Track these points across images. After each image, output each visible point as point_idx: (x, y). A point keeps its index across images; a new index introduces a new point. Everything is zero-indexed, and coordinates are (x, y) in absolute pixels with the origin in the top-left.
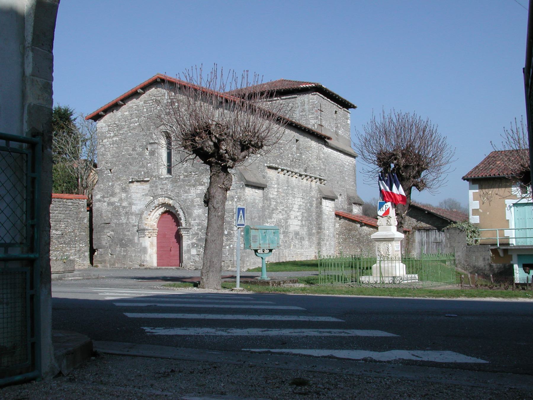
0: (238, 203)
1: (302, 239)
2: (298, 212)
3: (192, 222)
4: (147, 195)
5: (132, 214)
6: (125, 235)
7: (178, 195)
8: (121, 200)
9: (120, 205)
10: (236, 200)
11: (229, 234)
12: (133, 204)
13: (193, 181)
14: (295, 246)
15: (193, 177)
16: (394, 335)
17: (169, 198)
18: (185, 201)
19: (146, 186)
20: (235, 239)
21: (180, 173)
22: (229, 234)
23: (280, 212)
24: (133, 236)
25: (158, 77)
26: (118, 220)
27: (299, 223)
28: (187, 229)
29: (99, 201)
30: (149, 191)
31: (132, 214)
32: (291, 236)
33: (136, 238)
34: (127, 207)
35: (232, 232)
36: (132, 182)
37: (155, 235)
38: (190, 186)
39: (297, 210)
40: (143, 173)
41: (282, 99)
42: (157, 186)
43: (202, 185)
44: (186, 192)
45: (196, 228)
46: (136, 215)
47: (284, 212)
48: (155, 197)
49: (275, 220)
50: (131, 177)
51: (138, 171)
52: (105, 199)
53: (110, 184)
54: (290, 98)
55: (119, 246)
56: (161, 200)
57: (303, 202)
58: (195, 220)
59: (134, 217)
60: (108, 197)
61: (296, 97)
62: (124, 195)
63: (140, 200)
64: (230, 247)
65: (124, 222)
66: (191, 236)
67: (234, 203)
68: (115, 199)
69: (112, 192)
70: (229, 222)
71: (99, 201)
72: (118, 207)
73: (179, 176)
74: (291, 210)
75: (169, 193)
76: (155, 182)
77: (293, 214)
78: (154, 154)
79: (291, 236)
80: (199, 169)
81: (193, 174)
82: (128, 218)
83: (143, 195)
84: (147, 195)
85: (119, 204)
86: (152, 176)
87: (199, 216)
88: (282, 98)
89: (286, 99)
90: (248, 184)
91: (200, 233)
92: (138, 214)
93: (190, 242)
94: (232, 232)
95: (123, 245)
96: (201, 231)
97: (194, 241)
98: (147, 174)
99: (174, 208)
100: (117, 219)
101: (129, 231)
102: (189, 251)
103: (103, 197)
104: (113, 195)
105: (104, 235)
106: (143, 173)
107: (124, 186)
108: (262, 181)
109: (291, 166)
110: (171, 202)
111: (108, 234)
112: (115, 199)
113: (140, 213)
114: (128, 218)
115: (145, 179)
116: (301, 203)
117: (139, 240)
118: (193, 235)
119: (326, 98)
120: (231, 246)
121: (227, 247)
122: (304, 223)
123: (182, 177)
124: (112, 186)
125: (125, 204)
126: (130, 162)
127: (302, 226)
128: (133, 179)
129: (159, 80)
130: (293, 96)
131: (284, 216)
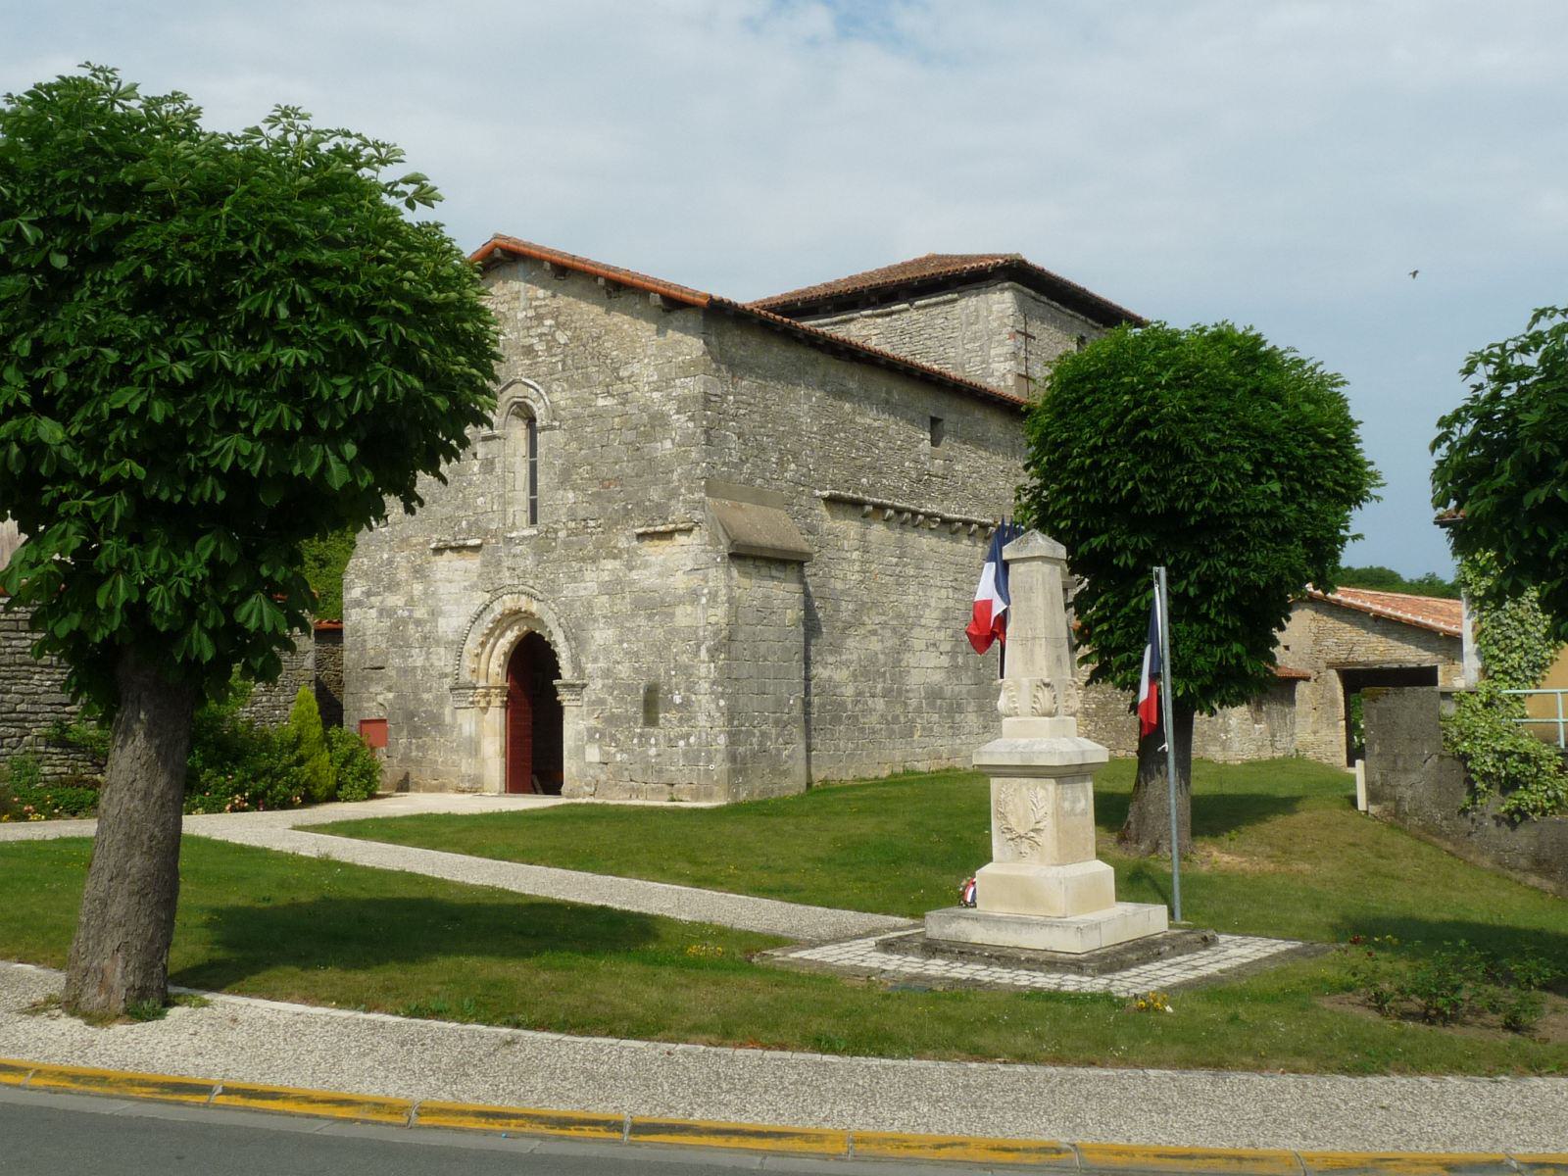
0: (711, 611)
1: (955, 708)
2: (939, 628)
3: (589, 667)
4: (473, 587)
5: (438, 642)
6: (420, 701)
7: (552, 589)
8: (411, 602)
9: (410, 617)
10: (704, 600)
11: (686, 704)
12: (441, 613)
13: (590, 547)
14: (931, 730)
15: (592, 534)
16: (1290, 945)
17: (530, 595)
18: (569, 605)
19: (473, 563)
20: (702, 721)
21: (556, 522)
22: (686, 704)
23: (874, 633)
24: (440, 700)
25: (496, 246)
26: (404, 657)
27: (945, 661)
28: (577, 688)
29: (358, 603)
30: (480, 575)
31: (438, 642)
32: (913, 703)
33: (447, 710)
34: (426, 622)
35: (693, 697)
36: (438, 551)
37: (497, 701)
38: (583, 559)
39: (937, 623)
40: (464, 523)
41: (918, 308)
42: (499, 563)
43: (615, 558)
44: (574, 579)
45: (599, 683)
46: (449, 644)
47: (888, 633)
48: (496, 592)
49: (855, 657)
50: (436, 536)
51: (450, 519)
52: (372, 599)
53: (385, 556)
54: (936, 304)
55: (405, 732)
56: (509, 602)
57: (957, 600)
58: (595, 660)
59: (442, 651)
60: (379, 594)
61: (955, 301)
62: (418, 588)
63: (457, 602)
64: (688, 744)
65: (419, 662)
66: (585, 708)
67: (699, 610)
68: (394, 600)
69: (391, 580)
70: (687, 667)
71: (358, 603)
72: (404, 622)
73: (556, 531)
74: (913, 625)
75: (531, 583)
76: (496, 549)
77: (918, 638)
78: (493, 469)
79: (913, 703)
80: (606, 509)
81: (592, 523)
82: (428, 653)
83: (465, 588)
84: (473, 587)
85: (406, 614)
86: (487, 532)
87: (606, 650)
88: (918, 303)
89: (926, 306)
90: (743, 551)
91: (610, 699)
92: (453, 642)
93: (582, 725)
94: (693, 697)
95: (415, 732)
96: (611, 694)
97: (593, 722)
98: (475, 527)
99: (540, 621)
100: (403, 657)
101: (429, 690)
102: (580, 751)
103: (368, 594)
104: (393, 586)
105: (369, 700)
106: (464, 523)
107: (419, 562)
108: (797, 541)
109: (912, 495)
110: (534, 607)
111: (380, 699)
112: (394, 600)
113: (456, 638)
114: (428, 653)
115: (470, 542)
116: (951, 603)
117: (453, 714)
118: (591, 703)
119: (1044, 299)
120: (692, 740)
121: (682, 743)
122: (960, 660)
123: (562, 534)
124: (390, 562)
125: (420, 613)
126: (433, 494)
127: (954, 670)
128: (440, 540)
129: (498, 253)
130: (946, 298)
131: (889, 644)
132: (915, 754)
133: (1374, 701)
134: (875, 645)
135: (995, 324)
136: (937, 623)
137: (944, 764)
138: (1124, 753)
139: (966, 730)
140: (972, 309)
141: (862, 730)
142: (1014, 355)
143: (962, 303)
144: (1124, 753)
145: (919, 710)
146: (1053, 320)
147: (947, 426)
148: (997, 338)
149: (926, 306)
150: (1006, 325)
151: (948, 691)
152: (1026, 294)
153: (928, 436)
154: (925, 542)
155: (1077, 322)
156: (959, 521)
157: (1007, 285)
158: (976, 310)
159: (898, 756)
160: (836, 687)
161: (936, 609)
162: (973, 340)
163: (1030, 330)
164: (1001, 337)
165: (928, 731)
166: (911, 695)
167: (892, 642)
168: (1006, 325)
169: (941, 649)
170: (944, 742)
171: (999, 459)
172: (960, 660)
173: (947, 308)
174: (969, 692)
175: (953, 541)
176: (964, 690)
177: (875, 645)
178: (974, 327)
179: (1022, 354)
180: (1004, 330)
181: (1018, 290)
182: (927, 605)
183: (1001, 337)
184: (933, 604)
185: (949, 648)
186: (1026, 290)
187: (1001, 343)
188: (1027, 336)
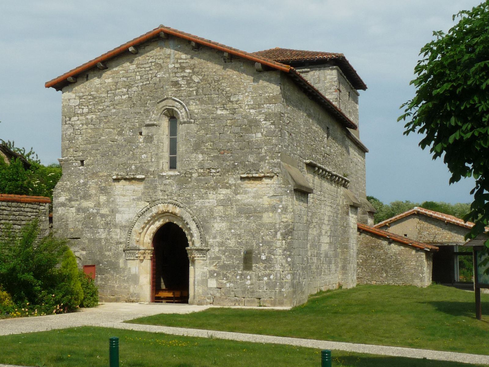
61: (308, 72)
135: (328, 85)
138: (375, 282)
140: (317, 76)
148: (329, 91)
150: (333, 85)
157: (335, 67)
158: (319, 77)
164: (331, 91)
168: (333, 85)
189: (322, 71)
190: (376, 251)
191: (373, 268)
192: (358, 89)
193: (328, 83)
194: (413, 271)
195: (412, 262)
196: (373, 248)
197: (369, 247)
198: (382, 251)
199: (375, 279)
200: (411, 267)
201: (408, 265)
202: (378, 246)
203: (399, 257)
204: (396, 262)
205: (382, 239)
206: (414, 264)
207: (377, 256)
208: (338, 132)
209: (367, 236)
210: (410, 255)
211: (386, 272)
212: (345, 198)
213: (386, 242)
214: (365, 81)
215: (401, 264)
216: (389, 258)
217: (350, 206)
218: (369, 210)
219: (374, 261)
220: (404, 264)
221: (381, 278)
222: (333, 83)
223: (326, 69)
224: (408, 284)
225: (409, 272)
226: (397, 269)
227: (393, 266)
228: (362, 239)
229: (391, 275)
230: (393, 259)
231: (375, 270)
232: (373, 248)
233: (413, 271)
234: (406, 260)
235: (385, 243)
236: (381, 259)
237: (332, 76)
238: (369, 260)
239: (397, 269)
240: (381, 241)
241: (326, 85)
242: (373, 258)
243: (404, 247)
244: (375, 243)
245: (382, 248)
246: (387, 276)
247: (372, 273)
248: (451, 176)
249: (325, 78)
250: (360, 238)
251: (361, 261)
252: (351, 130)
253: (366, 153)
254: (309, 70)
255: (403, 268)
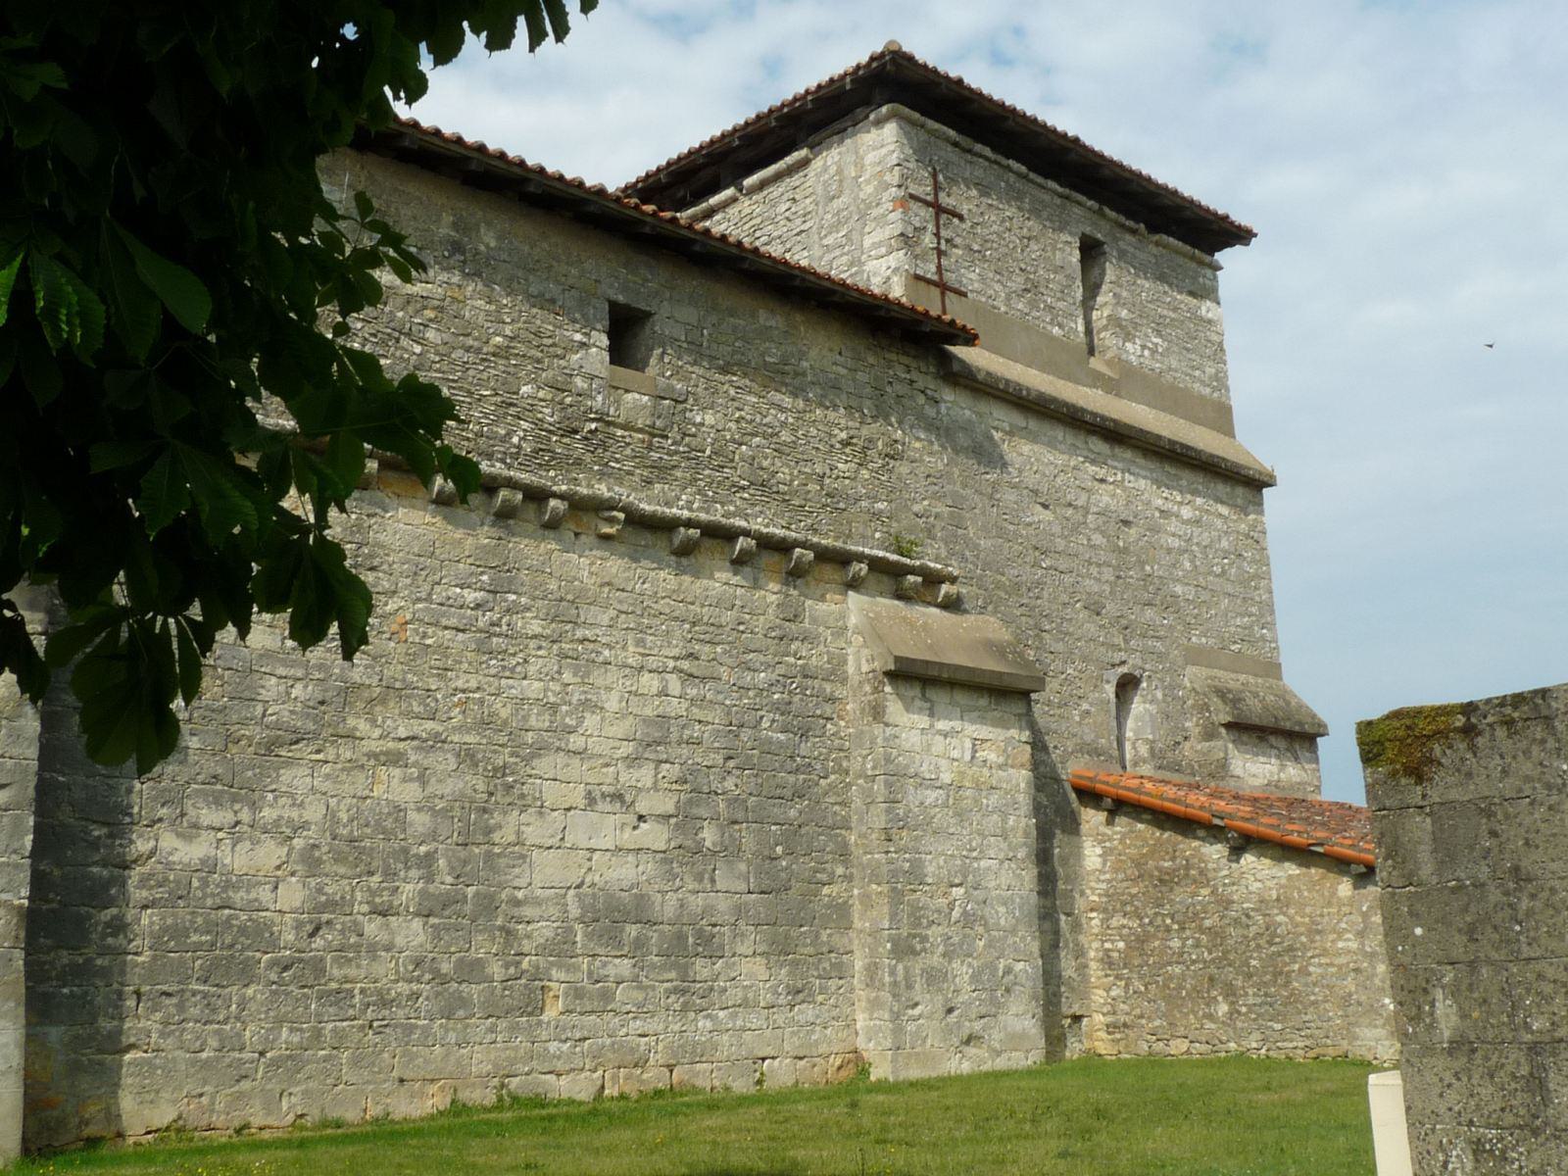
1: (691, 943)
2: (633, 761)
14: (607, 996)
27: (655, 835)
49: (314, 812)
54: (778, 177)
61: (804, 163)
74: (539, 750)
89: (763, 185)
109: (542, 456)
116: (675, 707)
132: (545, 1056)
133: (1417, 773)
134: (394, 787)
135: (869, 189)
136: (627, 749)
137: (653, 1077)
138: (1184, 1045)
139: (735, 995)
140: (833, 170)
141: (341, 997)
142: (906, 240)
143: (817, 164)
144: (1184, 1045)
145: (560, 949)
146: (1014, 196)
147: (660, 325)
148: (875, 212)
149: (763, 185)
150: (888, 186)
151: (667, 906)
152: (931, 132)
153: (605, 341)
154: (587, 566)
155: (1077, 210)
156: (689, 524)
157: (884, 109)
158: (839, 172)
159: (480, 1060)
160: (228, 885)
161: (621, 715)
162: (835, 228)
163: (945, 200)
164: (880, 210)
165: (596, 998)
166: (528, 912)
167: (453, 783)
168: (888, 186)
169: (642, 807)
170: (653, 1025)
171: (838, 416)
172: (709, 836)
173: (796, 180)
174: (739, 911)
175: (680, 571)
176: (723, 904)
177: (394, 787)
178: (836, 204)
179: (928, 240)
180: (886, 196)
181: (913, 123)
182: (588, 705)
183: (880, 210)
184: (612, 703)
185: (668, 805)
186: (932, 124)
187: (881, 221)
188: (939, 209)
189: (848, 141)
190: (1180, 895)
191: (1171, 978)
192: (1220, 249)
193: (868, 182)
194: (1350, 984)
195: (1340, 934)
196: (1167, 880)
197: (1152, 876)
198: (1205, 891)
199: (1182, 1031)
200: (1342, 960)
201: (1325, 953)
202: (1187, 867)
203: (1280, 918)
204: (1271, 943)
205: (1201, 833)
206: (1354, 945)
207: (1189, 919)
208: (901, 370)
209: (1140, 826)
210: (1329, 904)
211: (1230, 993)
212: (865, 645)
213: (1219, 846)
214: (1240, 218)
215: (1291, 949)
216: (1236, 922)
217: (889, 674)
218: (1229, 719)
219: (1176, 943)
220: (1304, 947)
221: (1209, 1025)
222: (888, 178)
223: (859, 132)
224: (1331, 1051)
225: (1330, 987)
226: (1277, 974)
227: (1265, 966)
228: (1122, 841)
229: (1250, 1007)
230: (1253, 930)
231: (1180, 987)
232: (1167, 880)
233: (1350, 984)
234: (1314, 931)
235: (1216, 852)
236: (1201, 930)
237: (884, 151)
238: (1154, 936)
239: (1277, 974)
240: (1196, 843)
241: (862, 195)
242: (1168, 930)
243: (1300, 865)
244: (1173, 859)
245: (1204, 878)
246: (1234, 1013)
247: (1168, 999)
248: (422, 124)
249: (860, 165)
250: (1110, 839)
251: (1121, 945)
252: (959, 351)
253: (1265, 490)
254: (803, 153)
255: (1304, 972)
